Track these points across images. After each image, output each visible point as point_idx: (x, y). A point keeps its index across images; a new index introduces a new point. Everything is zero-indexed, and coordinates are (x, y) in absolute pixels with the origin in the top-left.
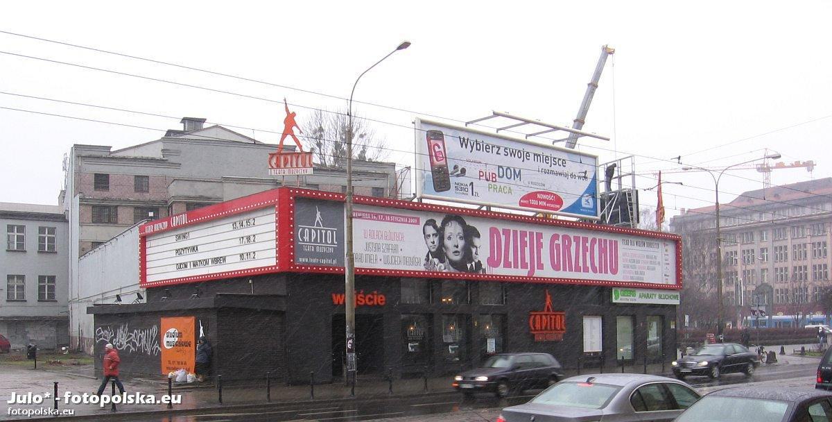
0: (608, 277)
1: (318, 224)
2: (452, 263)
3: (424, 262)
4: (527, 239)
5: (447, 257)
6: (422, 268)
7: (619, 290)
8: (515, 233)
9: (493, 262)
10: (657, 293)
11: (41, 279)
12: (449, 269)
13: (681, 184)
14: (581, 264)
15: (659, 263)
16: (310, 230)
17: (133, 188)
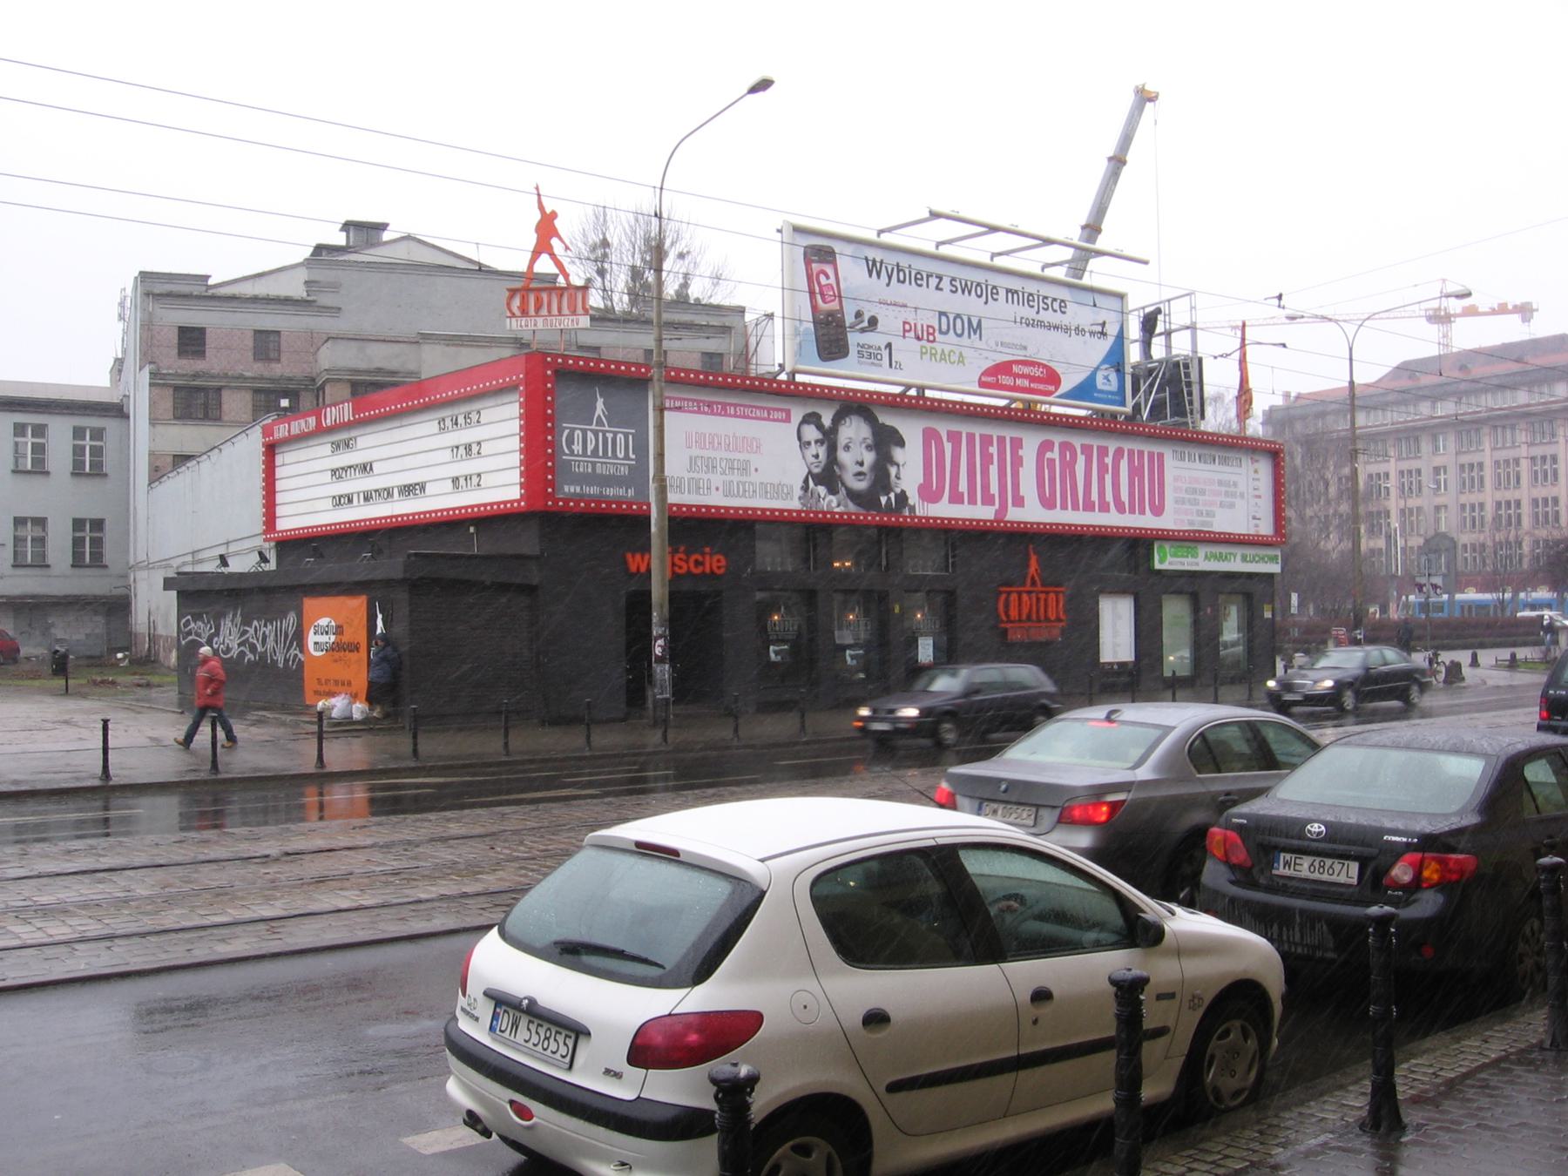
0: (1145, 521)
1: (600, 423)
2: (853, 495)
3: (798, 492)
4: (993, 450)
5: (843, 484)
6: (794, 504)
7: (1167, 546)
8: (971, 437)
9: (929, 493)
10: (1239, 551)
11: (78, 524)
12: (846, 506)
14: (1095, 496)
15: (1242, 495)
16: (584, 432)
17: (250, 354)
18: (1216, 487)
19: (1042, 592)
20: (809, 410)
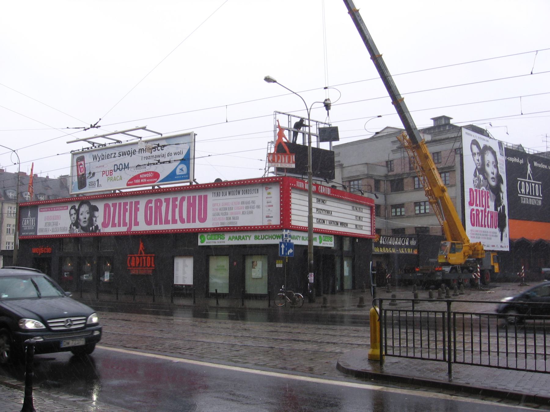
0: (197, 225)
1: (530, 179)
2: (83, 228)
3: (69, 229)
4: (128, 207)
5: (80, 225)
6: (67, 232)
7: (206, 235)
9: (105, 225)
10: (253, 235)
12: (81, 231)
15: (258, 207)
16: (525, 182)
18: (240, 205)
19: (145, 256)
20: (73, 205)
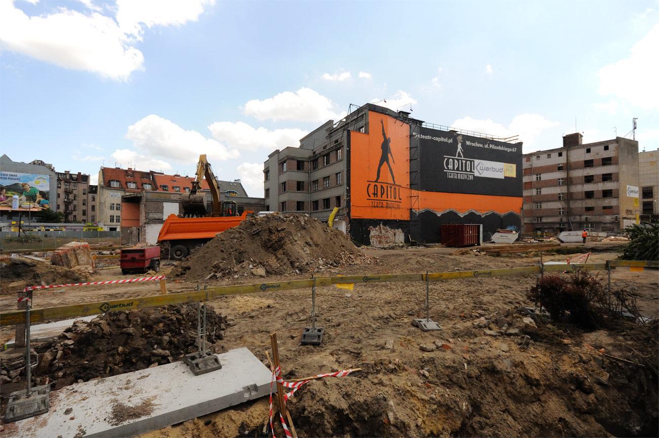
13: (635, 128)
16: (453, 159)
